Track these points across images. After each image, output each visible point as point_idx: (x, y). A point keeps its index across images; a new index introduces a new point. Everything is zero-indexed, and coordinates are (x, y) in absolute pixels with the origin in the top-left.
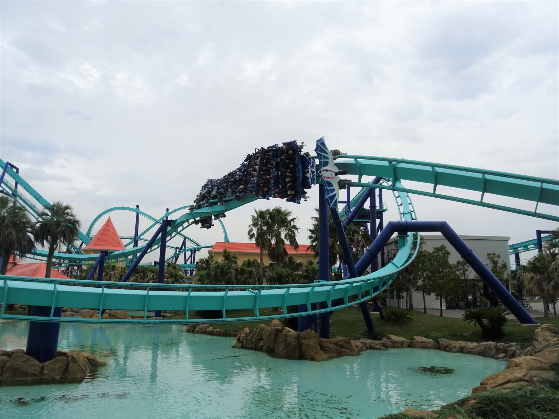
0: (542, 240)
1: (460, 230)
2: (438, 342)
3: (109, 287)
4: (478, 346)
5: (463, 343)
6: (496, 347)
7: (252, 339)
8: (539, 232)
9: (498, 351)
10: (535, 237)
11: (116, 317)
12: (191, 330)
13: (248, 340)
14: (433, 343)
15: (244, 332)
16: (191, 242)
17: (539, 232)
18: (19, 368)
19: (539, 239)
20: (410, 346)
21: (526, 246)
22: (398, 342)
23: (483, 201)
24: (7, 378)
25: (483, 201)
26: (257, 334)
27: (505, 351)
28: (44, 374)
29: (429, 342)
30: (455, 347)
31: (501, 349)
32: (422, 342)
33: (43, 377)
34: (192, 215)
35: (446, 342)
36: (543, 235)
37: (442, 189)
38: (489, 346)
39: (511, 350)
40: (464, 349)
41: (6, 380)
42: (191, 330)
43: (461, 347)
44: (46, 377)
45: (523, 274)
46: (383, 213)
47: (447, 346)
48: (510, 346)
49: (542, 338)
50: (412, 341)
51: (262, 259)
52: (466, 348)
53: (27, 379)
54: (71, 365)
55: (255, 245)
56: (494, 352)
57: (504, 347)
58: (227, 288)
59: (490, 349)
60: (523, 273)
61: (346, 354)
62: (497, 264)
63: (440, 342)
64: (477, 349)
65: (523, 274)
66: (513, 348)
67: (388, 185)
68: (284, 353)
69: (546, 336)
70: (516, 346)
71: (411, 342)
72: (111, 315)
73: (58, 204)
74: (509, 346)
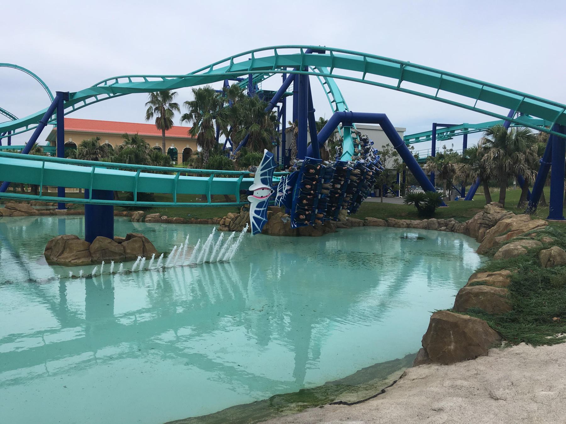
0: (437, 132)
1: (395, 122)
2: (387, 221)
3: (144, 171)
4: (421, 223)
5: (408, 221)
6: (439, 223)
7: (240, 223)
8: (435, 125)
9: (440, 224)
10: (431, 129)
11: (17, 210)
12: (141, 220)
13: (236, 224)
14: (383, 222)
15: (229, 217)
16: (9, 117)
17: (435, 125)
18: (108, 249)
19: (434, 131)
20: (364, 225)
21: (418, 138)
22: (355, 222)
23: (437, 96)
24: (99, 258)
25: (437, 96)
26: (245, 218)
27: (446, 225)
28: (128, 253)
29: (380, 221)
30: (403, 224)
31: (443, 224)
32: (374, 222)
33: (127, 256)
34: (112, 90)
35: (394, 220)
36: (438, 128)
37: (370, 77)
38: (433, 221)
39: (451, 224)
40: (410, 225)
41: (97, 259)
42: (141, 220)
43: (407, 224)
44: (129, 256)
45: (431, 164)
46: (287, 98)
47: (396, 224)
48: (450, 221)
49: (493, 211)
50: (366, 221)
51: (165, 144)
52: (412, 224)
53: (115, 258)
54: (146, 244)
55: (156, 128)
56: (437, 226)
57: (444, 222)
58: (213, 173)
59: (434, 224)
60: (431, 163)
61: (328, 232)
62: (442, 155)
63: (389, 221)
64: (421, 225)
65: (431, 164)
66: (453, 222)
67: (311, 66)
68: (282, 232)
69: (496, 209)
70: (455, 221)
71: (365, 222)
72: (9, 208)
73: (208, 88)
74: (449, 221)
